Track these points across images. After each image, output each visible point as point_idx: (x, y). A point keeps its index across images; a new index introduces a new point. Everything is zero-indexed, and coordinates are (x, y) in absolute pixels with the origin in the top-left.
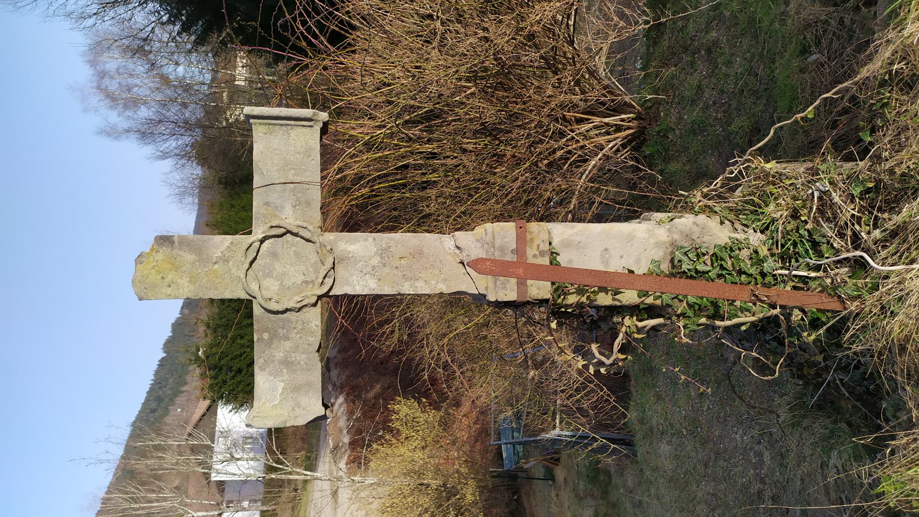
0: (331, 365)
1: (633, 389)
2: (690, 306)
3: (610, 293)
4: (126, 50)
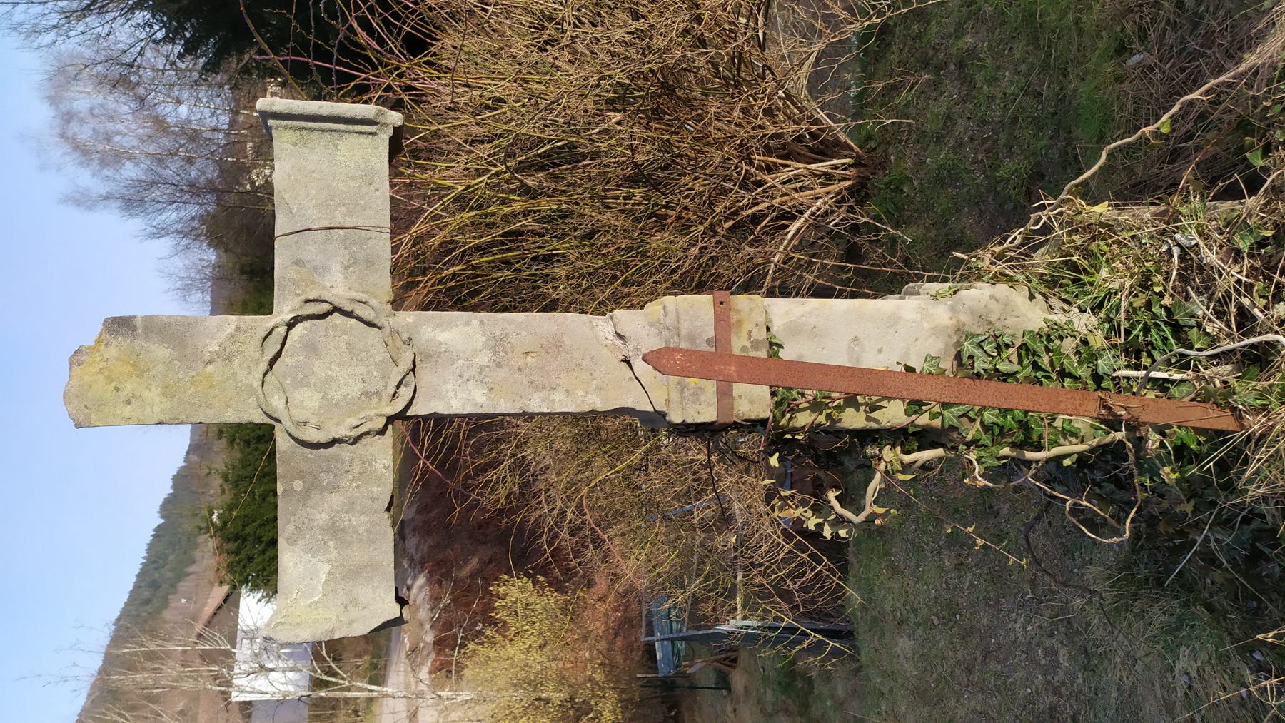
0: (407, 531)
1: (852, 559)
2: (987, 428)
3: (862, 408)
4: (101, 81)
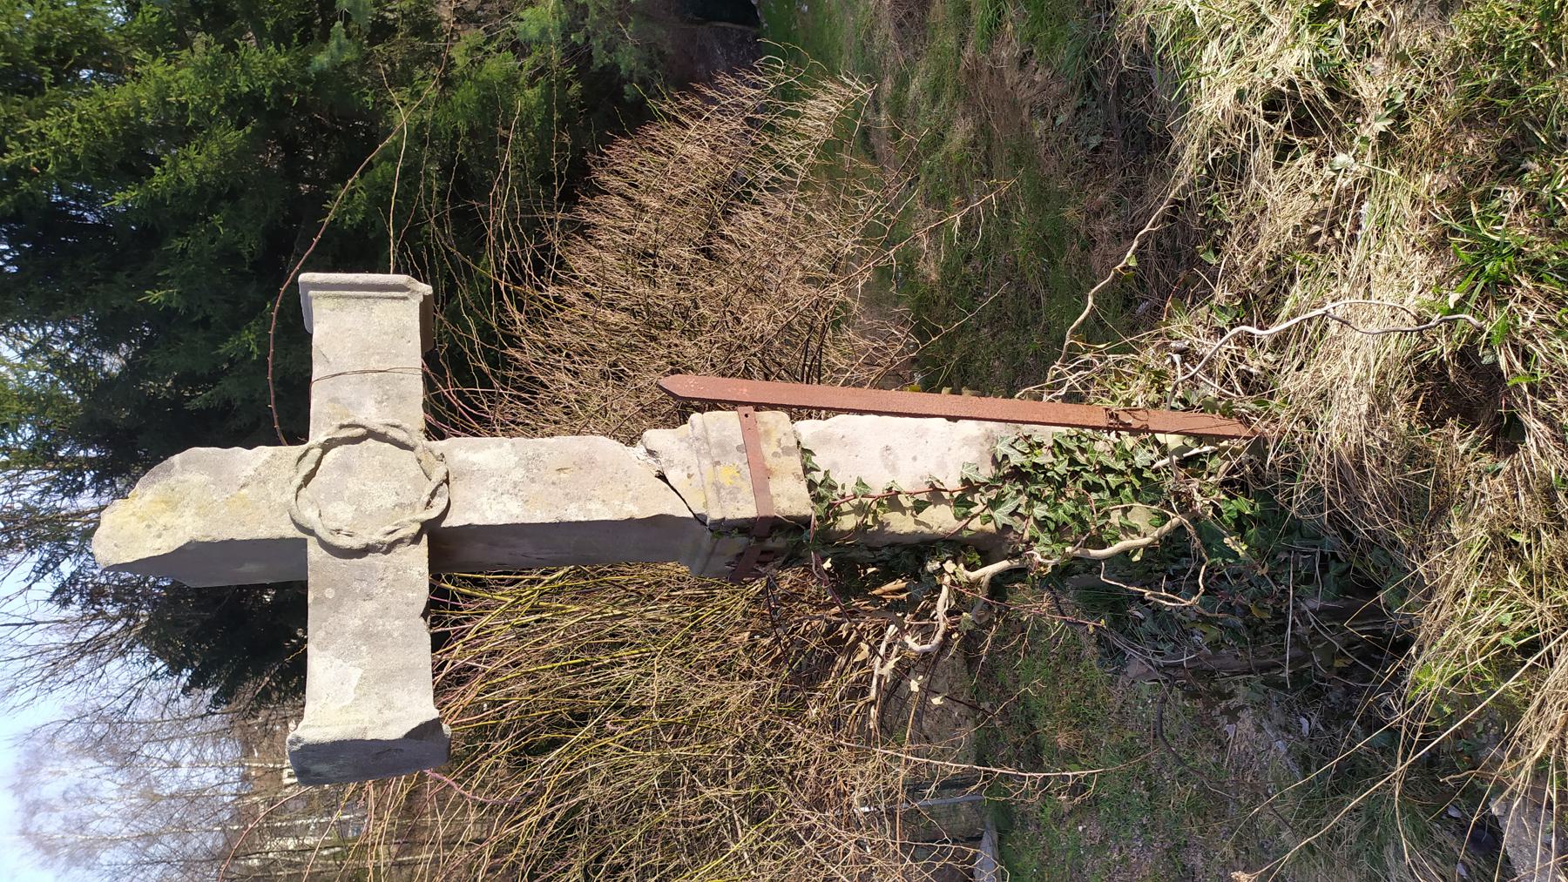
3: (908, 513)
